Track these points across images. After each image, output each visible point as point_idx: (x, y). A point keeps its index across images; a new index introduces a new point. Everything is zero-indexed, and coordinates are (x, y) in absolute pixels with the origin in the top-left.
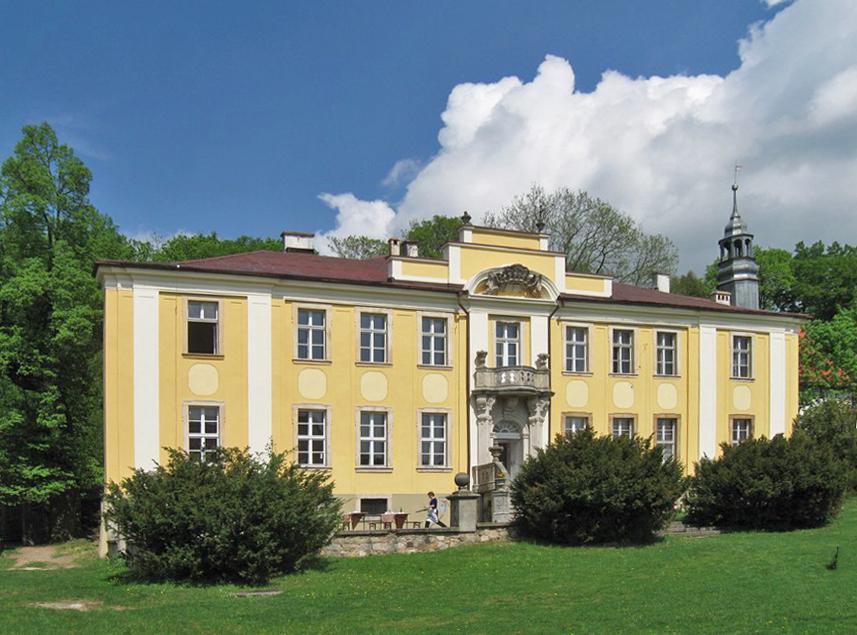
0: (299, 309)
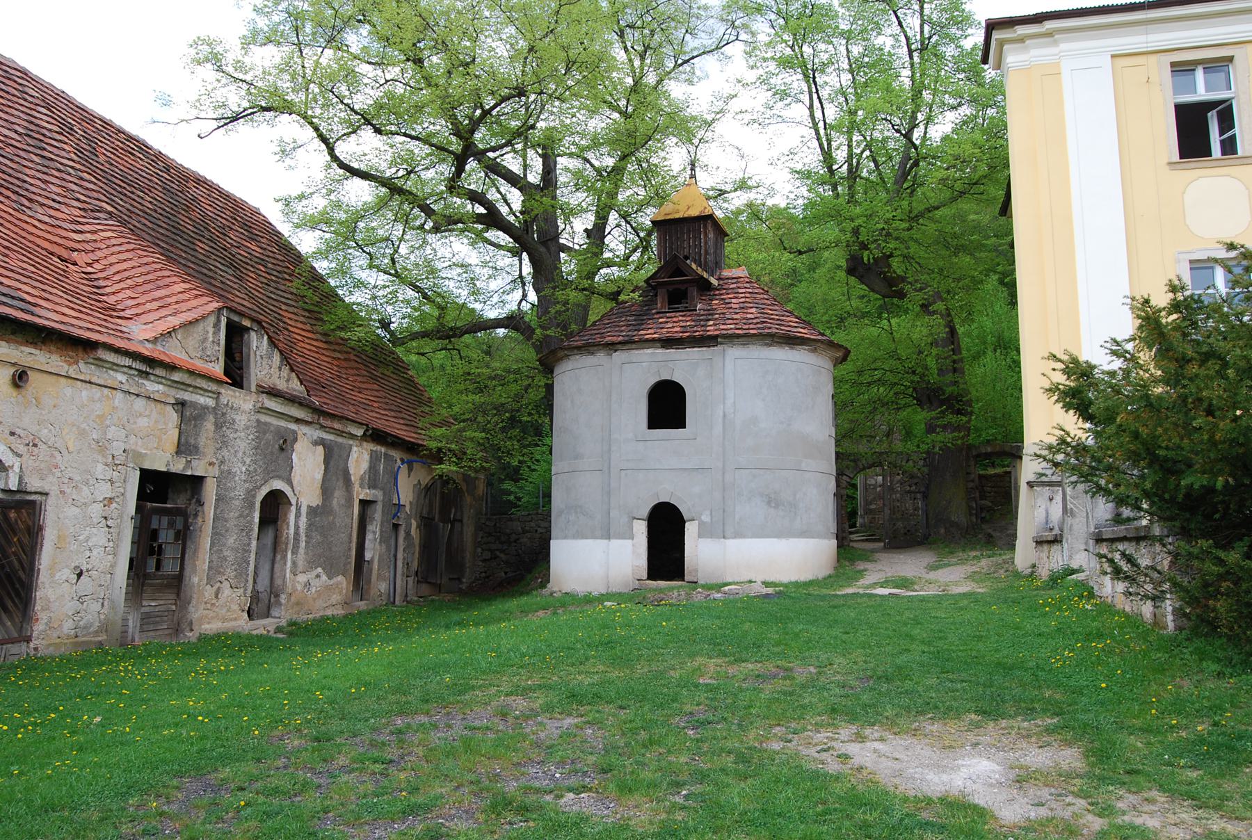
0: (1173, 64)
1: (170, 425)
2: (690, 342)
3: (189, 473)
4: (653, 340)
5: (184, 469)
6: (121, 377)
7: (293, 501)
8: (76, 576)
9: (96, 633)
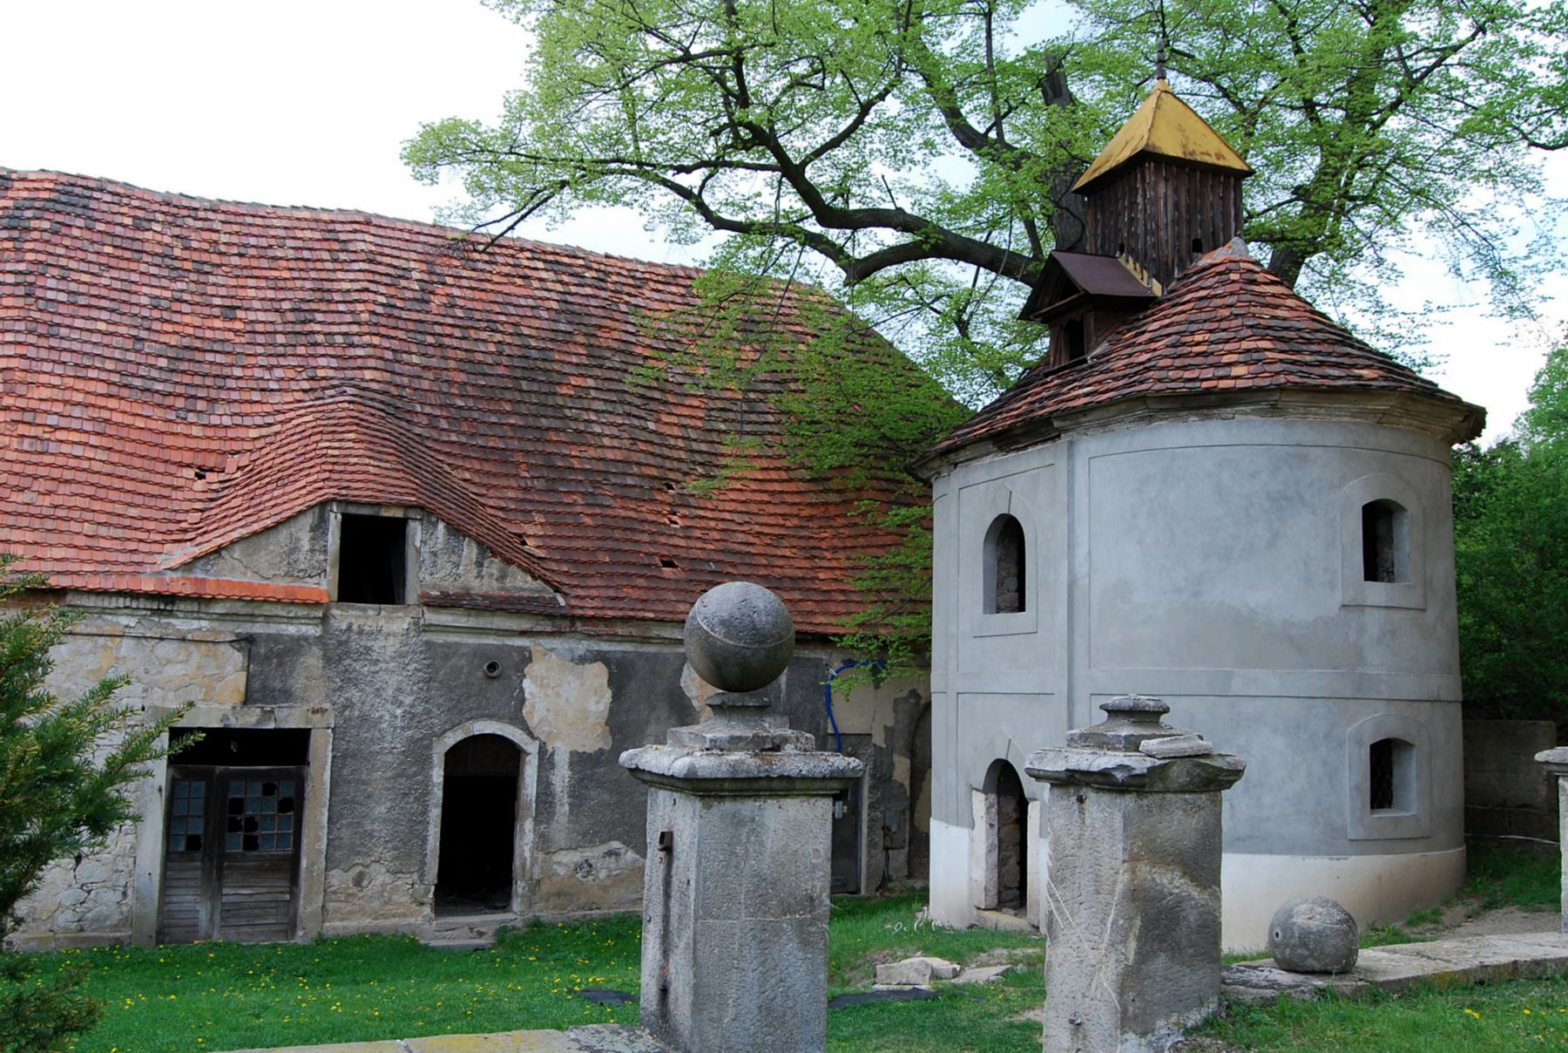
1: (229, 668)
2: (1026, 434)
3: (271, 726)
4: (980, 440)
5: (258, 722)
6: (124, 620)
7: (531, 748)
8: (74, 861)
9: (115, 927)
